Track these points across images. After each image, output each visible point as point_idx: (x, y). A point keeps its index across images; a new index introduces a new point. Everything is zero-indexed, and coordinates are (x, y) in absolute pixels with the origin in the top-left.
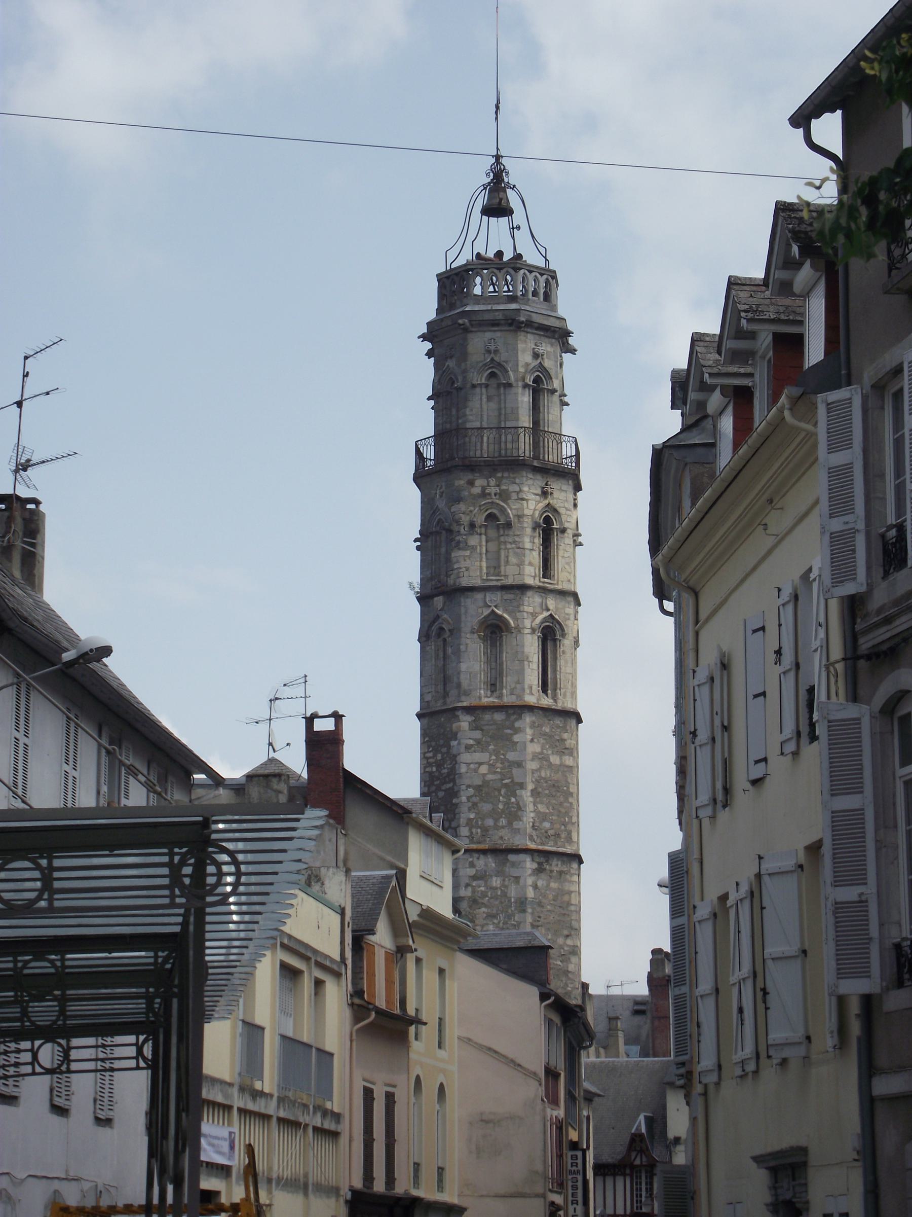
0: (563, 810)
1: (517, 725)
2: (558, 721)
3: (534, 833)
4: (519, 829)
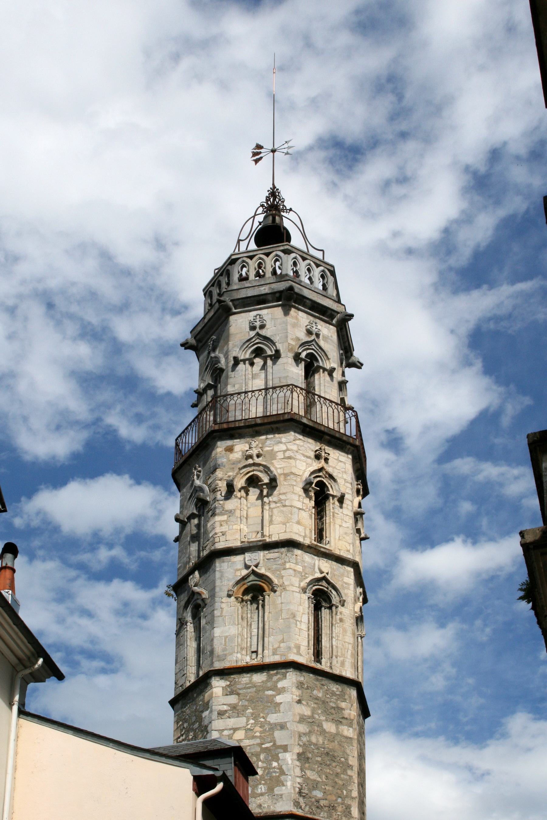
0: (340, 782)
1: (280, 685)
2: (335, 687)
3: (301, 800)
4: (281, 795)
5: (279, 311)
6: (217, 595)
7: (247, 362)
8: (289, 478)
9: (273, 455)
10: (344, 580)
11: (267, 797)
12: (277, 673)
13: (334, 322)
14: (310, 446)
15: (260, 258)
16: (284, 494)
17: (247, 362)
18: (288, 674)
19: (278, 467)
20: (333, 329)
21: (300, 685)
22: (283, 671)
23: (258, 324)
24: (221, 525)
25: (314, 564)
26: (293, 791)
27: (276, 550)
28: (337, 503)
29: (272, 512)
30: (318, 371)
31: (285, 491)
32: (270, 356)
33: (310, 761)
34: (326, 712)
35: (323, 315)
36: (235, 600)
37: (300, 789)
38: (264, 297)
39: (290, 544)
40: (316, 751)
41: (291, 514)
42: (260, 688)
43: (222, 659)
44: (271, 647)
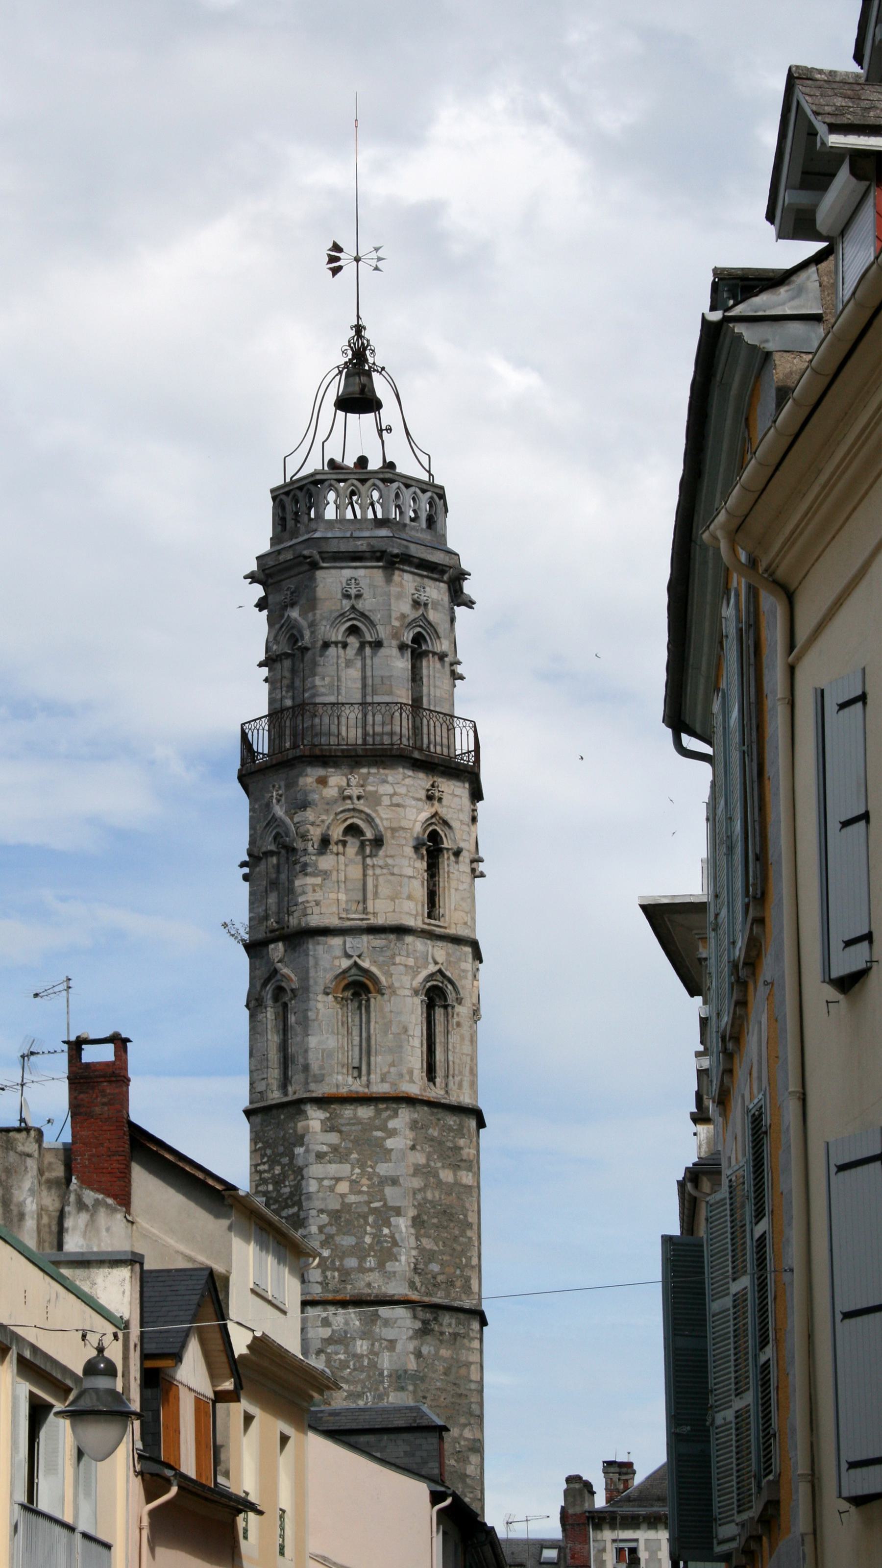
0: (459, 1248)
1: (391, 1124)
2: (452, 1120)
3: (417, 1279)
4: (395, 1273)
5: (378, 575)
6: (311, 989)
7: (340, 645)
8: (397, 834)
9: (375, 799)
10: (462, 967)
11: (377, 1274)
12: (387, 1109)
13: (445, 578)
14: (420, 782)
15: (353, 485)
16: (391, 856)
17: (340, 645)
18: (400, 1111)
19: (384, 817)
20: (443, 586)
21: (414, 1125)
22: (394, 1106)
23: (353, 592)
24: (314, 891)
25: (428, 951)
26: (407, 1269)
27: (383, 936)
28: (452, 858)
29: (377, 879)
30: (427, 656)
31: (392, 853)
32: (370, 643)
33: (426, 1225)
34: (442, 1157)
35: (432, 572)
36: (333, 999)
37: (415, 1265)
38: (361, 554)
39: (401, 931)
40: (432, 1211)
41: (401, 886)
42: (368, 1127)
43: (319, 1079)
44: (378, 1071)
